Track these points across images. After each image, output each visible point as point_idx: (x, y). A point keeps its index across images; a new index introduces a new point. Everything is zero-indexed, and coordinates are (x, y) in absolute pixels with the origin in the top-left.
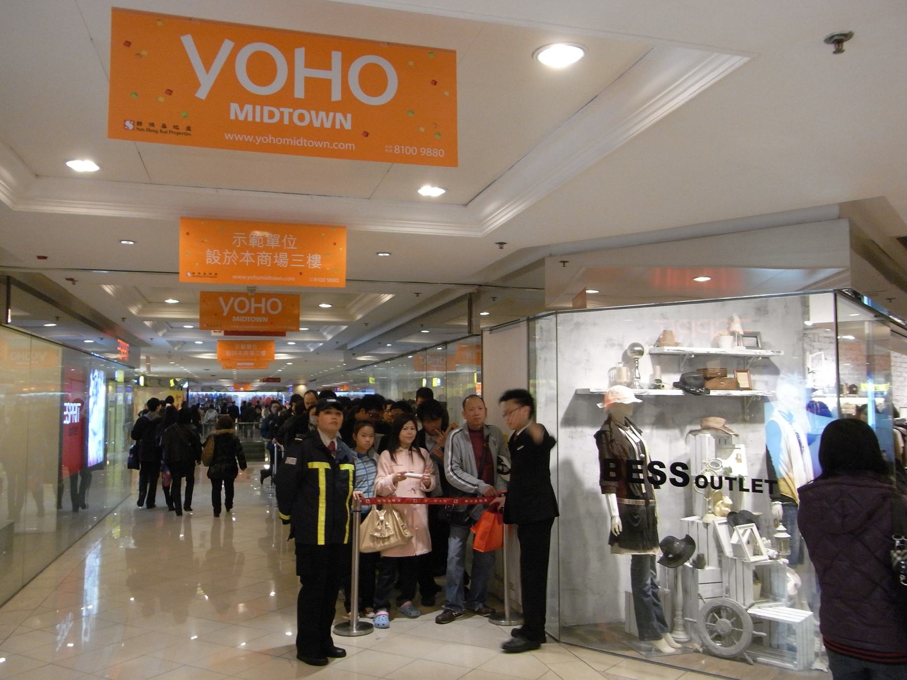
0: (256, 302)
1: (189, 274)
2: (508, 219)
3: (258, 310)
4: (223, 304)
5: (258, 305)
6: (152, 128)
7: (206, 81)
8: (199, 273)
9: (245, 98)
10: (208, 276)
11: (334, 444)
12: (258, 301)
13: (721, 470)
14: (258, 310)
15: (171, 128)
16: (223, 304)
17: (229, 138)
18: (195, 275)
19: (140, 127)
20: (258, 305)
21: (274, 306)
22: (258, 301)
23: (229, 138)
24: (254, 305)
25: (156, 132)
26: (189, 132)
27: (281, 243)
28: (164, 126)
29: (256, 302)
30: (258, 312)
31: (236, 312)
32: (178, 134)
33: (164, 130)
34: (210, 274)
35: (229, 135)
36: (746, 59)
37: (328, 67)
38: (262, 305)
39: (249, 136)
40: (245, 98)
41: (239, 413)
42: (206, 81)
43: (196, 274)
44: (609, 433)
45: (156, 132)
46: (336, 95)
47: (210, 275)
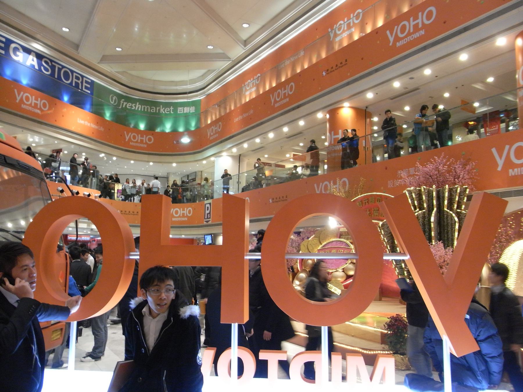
3: (142, 141)
5: (142, 138)
7: (127, 138)
8: (126, 211)
9: (132, 142)
10: (132, 214)
13: (86, 122)
14: (142, 141)
15: (131, 213)
17: (513, 170)
19: (328, 72)
20: (142, 138)
22: (142, 136)
23: (513, 170)
24: (140, 138)
25: (127, 214)
26: (346, 63)
28: (129, 212)
31: (132, 140)
33: (129, 213)
34: (133, 212)
37: (140, 139)
40: (132, 142)
41: (166, 372)
42: (127, 138)
43: (123, 212)
45: (127, 214)
46: (144, 142)
47: (133, 213)
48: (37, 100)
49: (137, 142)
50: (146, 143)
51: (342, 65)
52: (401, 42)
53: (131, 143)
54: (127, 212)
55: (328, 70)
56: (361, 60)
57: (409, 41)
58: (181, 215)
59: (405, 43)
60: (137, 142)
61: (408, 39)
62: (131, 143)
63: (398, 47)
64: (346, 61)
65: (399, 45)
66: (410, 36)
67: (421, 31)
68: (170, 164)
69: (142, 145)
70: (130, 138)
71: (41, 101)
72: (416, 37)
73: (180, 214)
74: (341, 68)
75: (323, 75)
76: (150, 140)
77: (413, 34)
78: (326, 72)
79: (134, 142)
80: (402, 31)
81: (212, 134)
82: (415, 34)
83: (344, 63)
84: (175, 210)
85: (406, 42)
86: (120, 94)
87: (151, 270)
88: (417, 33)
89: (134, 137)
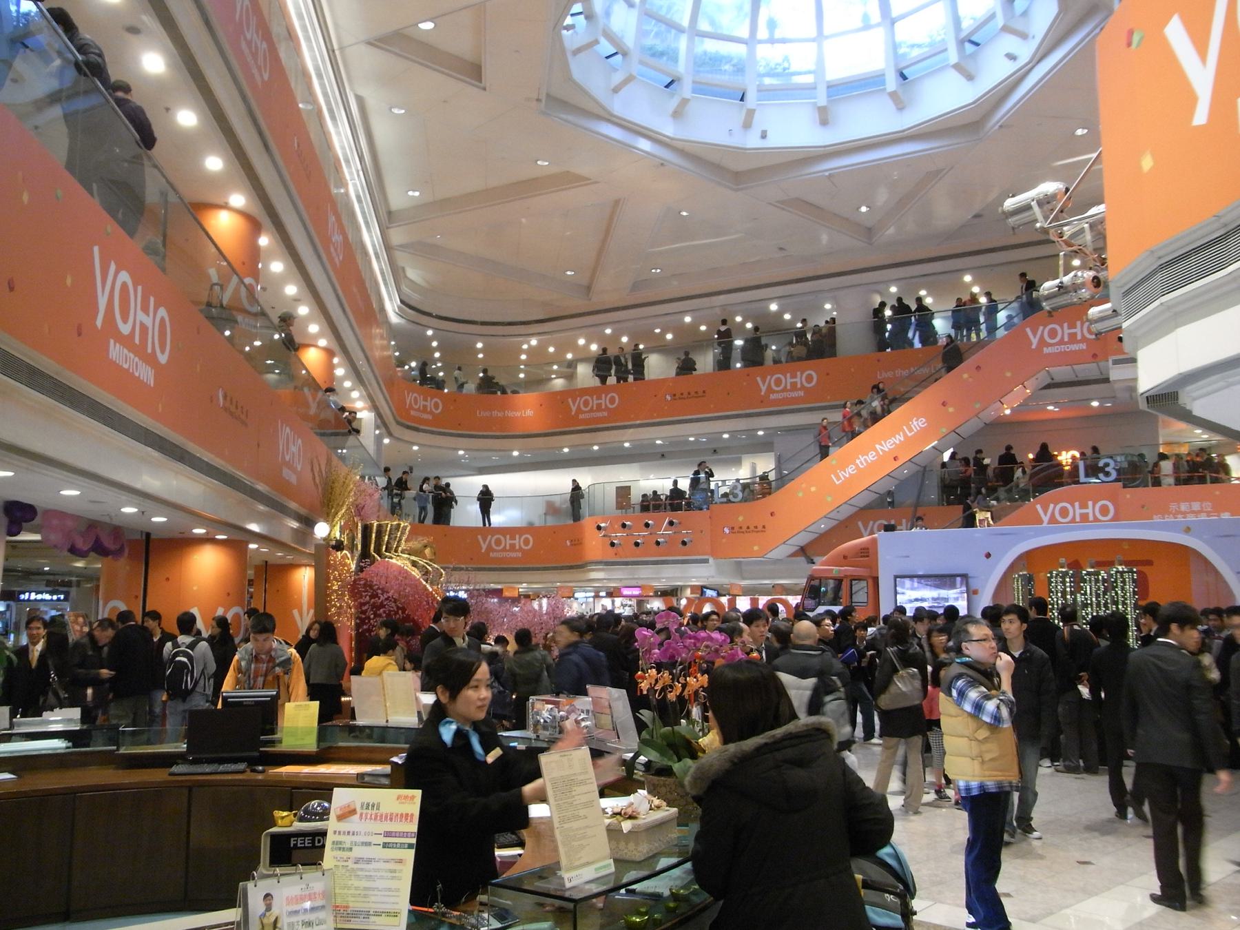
0: (515, 544)
1: (669, 398)
2: (1231, 372)
3: (425, 406)
4: (571, 404)
5: (513, 542)
8: (682, 394)
11: (127, 287)
12: (513, 538)
14: (599, 405)
16: (571, 404)
17: (900, 440)
18: (677, 397)
20: (513, 542)
21: (526, 542)
22: (513, 538)
23: (900, 440)
27: (1202, 507)
28: (689, 394)
29: (515, 544)
30: (513, 547)
32: (758, 532)
35: (897, 436)
36: (34, 664)
38: (516, 542)
39: (897, 436)
44: (27, 598)
46: (517, 547)
48: (426, 401)
49: (785, 390)
50: (607, 409)
54: (685, 395)
56: (899, 457)
58: (789, 387)
60: (785, 390)
64: (704, 392)
68: (882, 893)
69: (600, 414)
71: (431, 400)
73: (592, 407)
79: (778, 392)
84: (583, 399)
86: (343, 655)
87: (1145, 574)
89: (586, 403)
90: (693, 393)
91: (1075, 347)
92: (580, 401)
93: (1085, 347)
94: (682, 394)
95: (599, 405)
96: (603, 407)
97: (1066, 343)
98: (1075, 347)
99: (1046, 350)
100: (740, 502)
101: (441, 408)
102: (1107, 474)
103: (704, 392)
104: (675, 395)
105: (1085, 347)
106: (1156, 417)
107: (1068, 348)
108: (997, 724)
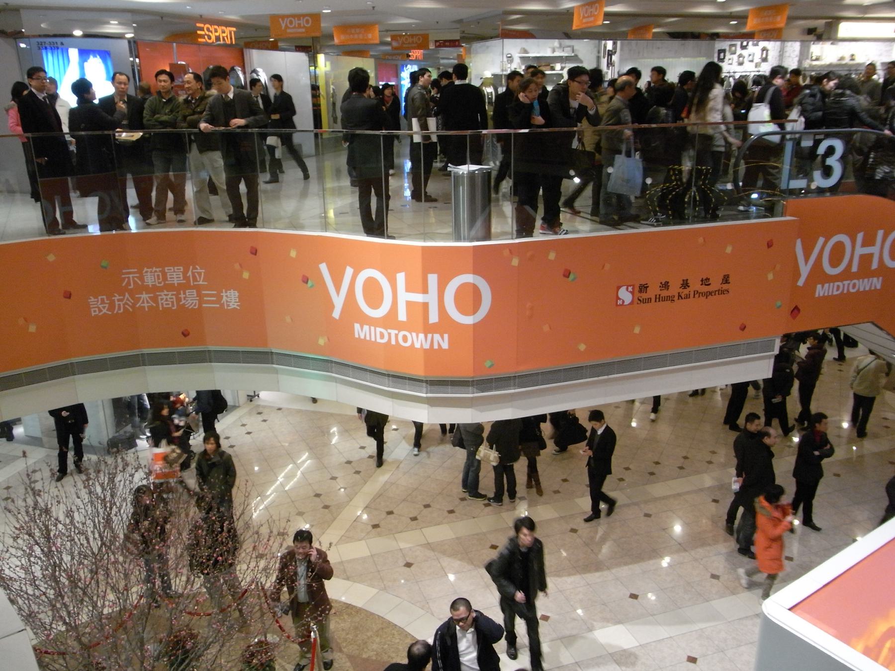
3: (299, 24)
6: (665, 293)
7: (283, 26)
14: (299, 24)
18: (651, 293)
19: (644, 296)
26: (725, 287)
40: (289, 28)
42: (283, 26)
49: (295, 27)
50: (304, 27)
51: (705, 289)
52: (826, 285)
53: (405, 46)
54: (675, 289)
55: (643, 288)
57: (845, 291)
59: (835, 293)
60: (295, 27)
61: (844, 285)
62: (405, 46)
63: (819, 297)
64: (726, 280)
65: (821, 295)
66: (851, 280)
67: (875, 279)
70: (286, 25)
72: (862, 289)
74: (703, 299)
75: (618, 298)
76: (307, 22)
77: (858, 279)
78: (637, 294)
80: (836, 259)
81: (586, 15)
82: (861, 280)
83: (716, 284)
85: (838, 292)
88: (866, 280)
89: (291, 22)
90: (695, 285)
91: (864, 285)
92: (287, 21)
93: (445, 345)
94: (666, 285)
95: (866, 259)
96: (875, 265)
97: (400, 326)
98: (864, 285)
99: (821, 291)
100: (833, 190)
101: (310, 22)
102: (827, 172)
103: (726, 280)
104: (643, 288)
105: (445, 345)
106: (266, 171)
107: (405, 339)
108: (376, 226)
